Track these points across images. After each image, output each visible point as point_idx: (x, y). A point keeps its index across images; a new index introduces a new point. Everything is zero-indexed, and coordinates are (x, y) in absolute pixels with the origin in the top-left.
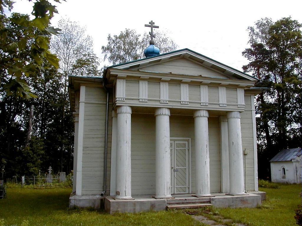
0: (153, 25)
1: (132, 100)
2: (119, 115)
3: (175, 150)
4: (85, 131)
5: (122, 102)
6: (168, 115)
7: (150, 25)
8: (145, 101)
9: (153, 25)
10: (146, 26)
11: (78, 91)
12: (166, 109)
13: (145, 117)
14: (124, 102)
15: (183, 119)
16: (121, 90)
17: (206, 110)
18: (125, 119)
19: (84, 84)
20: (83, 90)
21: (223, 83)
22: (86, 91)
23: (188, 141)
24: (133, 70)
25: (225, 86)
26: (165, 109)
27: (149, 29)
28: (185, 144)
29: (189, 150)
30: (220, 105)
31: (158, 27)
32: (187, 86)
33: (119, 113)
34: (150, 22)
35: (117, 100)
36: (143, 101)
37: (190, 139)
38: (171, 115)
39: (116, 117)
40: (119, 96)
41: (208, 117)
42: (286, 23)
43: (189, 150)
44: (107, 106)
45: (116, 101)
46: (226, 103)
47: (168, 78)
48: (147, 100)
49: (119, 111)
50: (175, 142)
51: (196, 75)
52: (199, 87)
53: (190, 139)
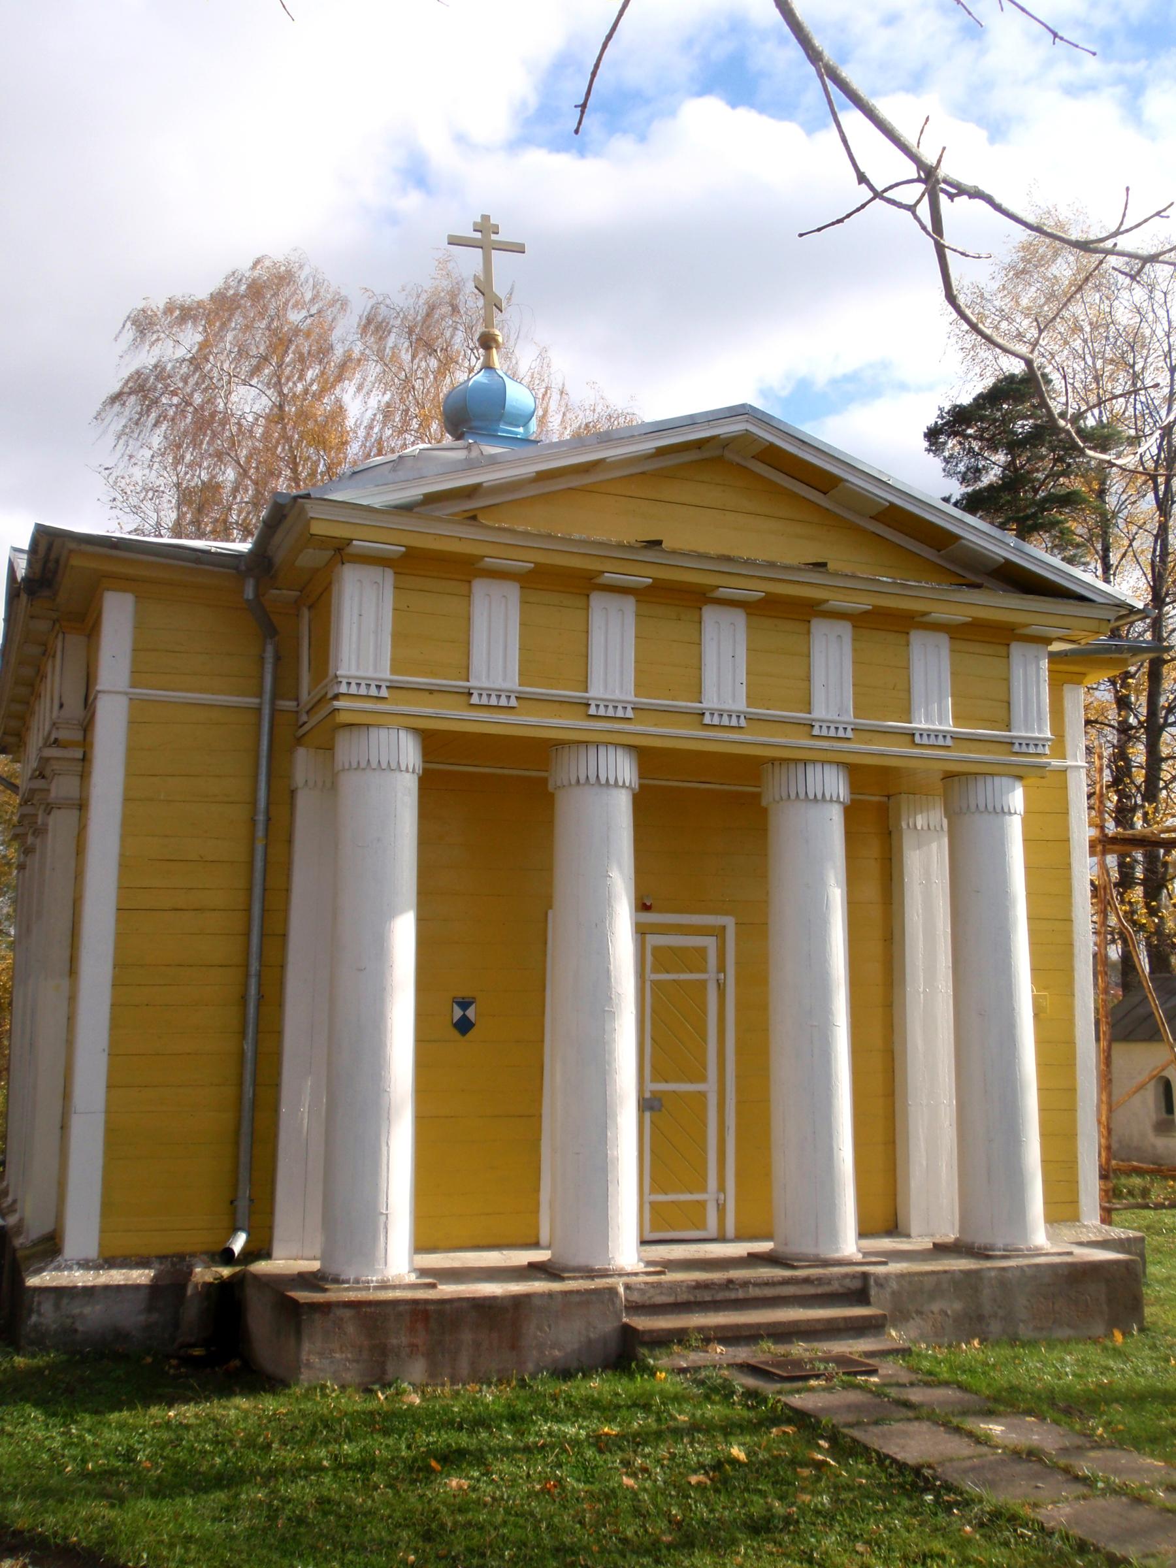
0: (494, 237)
1: (431, 692)
2: (348, 782)
3: (648, 984)
4: (126, 865)
5: (369, 705)
6: (838, 801)
7: (478, 235)
8: (503, 702)
9: (494, 237)
10: (454, 241)
11: (87, 623)
12: (620, 752)
13: (496, 802)
14: (381, 707)
15: (707, 819)
16: (365, 633)
17: (838, 764)
18: (386, 802)
19: (124, 582)
20: (118, 616)
21: (942, 613)
22: (139, 626)
23: (719, 933)
24: (437, 514)
25: (518, 581)
26: (611, 750)
27: (470, 261)
28: (702, 952)
29: (721, 988)
30: (917, 739)
31: (519, 249)
32: (943, 640)
33: (343, 770)
34: (479, 220)
35: (343, 689)
36: (494, 701)
37: (729, 922)
38: (641, 786)
39: (331, 786)
40: (354, 666)
41: (635, 784)
42: (734, 105)
43: (721, 988)
44: (259, 726)
45: (336, 697)
46: (632, 698)
47: (848, 599)
48: (384, 689)
49: (348, 749)
50: (648, 937)
51: (712, 552)
52: (1002, 650)
53: (729, 922)
